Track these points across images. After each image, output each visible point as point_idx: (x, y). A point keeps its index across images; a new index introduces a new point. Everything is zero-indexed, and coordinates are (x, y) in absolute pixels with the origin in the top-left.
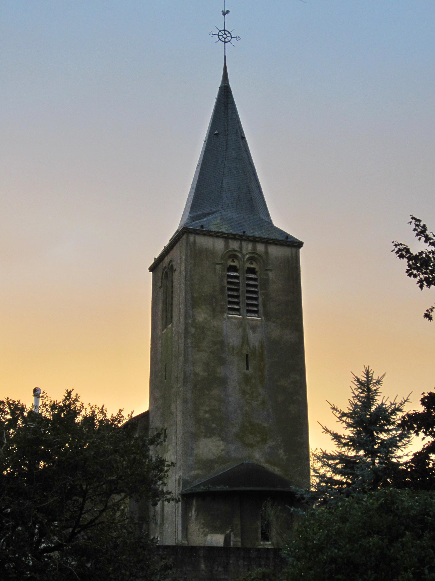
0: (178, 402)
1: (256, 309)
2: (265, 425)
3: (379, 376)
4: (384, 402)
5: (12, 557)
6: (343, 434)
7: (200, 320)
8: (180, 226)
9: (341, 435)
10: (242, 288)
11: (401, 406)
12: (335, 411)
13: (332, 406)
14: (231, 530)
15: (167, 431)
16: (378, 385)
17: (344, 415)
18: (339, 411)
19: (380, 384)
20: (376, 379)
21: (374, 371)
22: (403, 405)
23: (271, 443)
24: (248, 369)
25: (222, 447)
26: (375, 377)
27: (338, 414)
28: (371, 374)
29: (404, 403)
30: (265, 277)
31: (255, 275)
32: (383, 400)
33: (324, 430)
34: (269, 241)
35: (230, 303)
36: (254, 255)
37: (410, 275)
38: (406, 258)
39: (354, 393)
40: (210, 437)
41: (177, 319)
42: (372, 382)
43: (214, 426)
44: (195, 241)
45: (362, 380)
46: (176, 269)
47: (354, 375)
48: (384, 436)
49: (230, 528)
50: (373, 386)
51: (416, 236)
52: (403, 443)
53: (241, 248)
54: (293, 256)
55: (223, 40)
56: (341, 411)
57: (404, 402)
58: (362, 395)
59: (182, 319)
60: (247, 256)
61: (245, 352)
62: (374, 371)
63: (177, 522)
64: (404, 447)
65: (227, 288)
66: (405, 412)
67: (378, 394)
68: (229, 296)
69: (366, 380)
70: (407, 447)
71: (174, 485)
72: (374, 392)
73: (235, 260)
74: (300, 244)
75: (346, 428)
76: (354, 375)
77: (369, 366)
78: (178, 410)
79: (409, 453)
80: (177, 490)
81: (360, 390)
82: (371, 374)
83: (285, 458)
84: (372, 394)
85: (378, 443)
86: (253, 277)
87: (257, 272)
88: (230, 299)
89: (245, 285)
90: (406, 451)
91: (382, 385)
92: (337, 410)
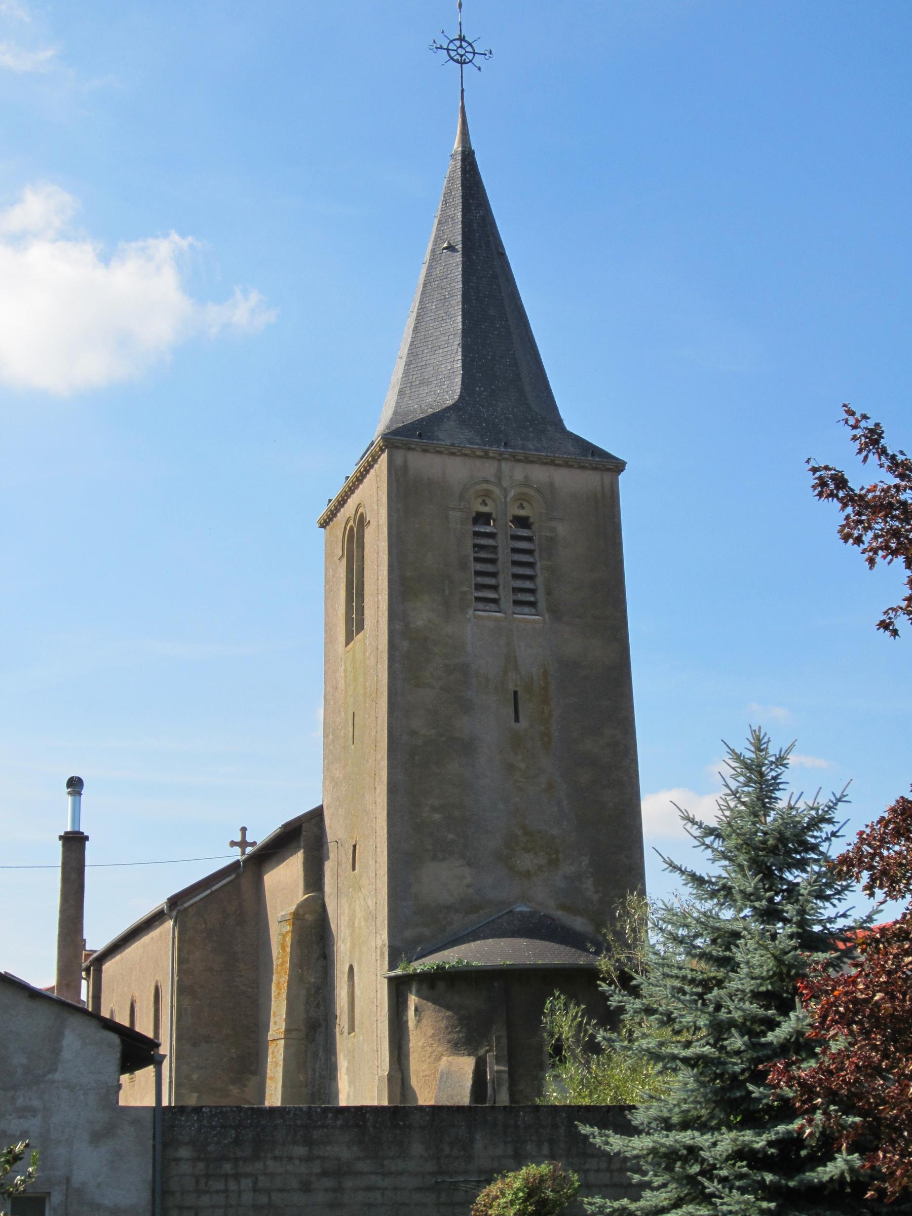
0: (378, 791)
1: (532, 599)
2: (555, 832)
3: (781, 749)
4: (792, 803)
6: (707, 874)
7: (420, 623)
8: (387, 431)
9: (702, 875)
10: (504, 556)
11: (830, 812)
12: (690, 824)
13: (683, 813)
14: (487, 1048)
15: (357, 846)
16: (780, 767)
17: (711, 831)
18: (699, 824)
19: (784, 765)
20: (775, 755)
21: (769, 738)
22: (832, 808)
23: (567, 869)
24: (517, 720)
25: (469, 880)
26: (773, 750)
27: (697, 829)
28: (764, 743)
29: (836, 804)
30: (548, 534)
31: (530, 531)
32: (790, 801)
33: (667, 866)
34: (557, 462)
35: (479, 587)
37: (846, 538)
38: (838, 499)
39: (727, 786)
40: (444, 859)
41: (374, 623)
42: (766, 762)
44: (405, 463)
45: (746, 757)
46: (369, 522)
47: (728, 746)
48: (795, 875)
49: (487, 1044)
50: (769, 770)
51: (858, 453)
52: (836, 889)
53: (499, 477)
55: (464, 44)
56: (701, 823)
57: (835, 801)
58: (746, 789)
59: (383, 622)
60: (512, 493)
61: (511, 687)
62: (769, 738)
63: (379, 1032)
64: (837, 897)
65: (472, 559)
66: (838, 822)
67: (781, 786)
68: (478, 573)
69: (753, 756)
70: (845, 897)
71: (374, 957)
72: (773, 781)
73: (488, 501)
74: (618, 466)
75: (714, 861)
76: (728, 746)
77: (760, 728)
78: (378, 807)
79: (848, 910)
80: (379, 969)
81: (742, 779)
82: (764, 743)
83: (596, 897)
84: (768, 786)
85: (783, 891)
86: (526, 535)
87: (532, 524)
89: (509, 551)
90: (841, 907)
91: (787, 766)
92: (693, 822)
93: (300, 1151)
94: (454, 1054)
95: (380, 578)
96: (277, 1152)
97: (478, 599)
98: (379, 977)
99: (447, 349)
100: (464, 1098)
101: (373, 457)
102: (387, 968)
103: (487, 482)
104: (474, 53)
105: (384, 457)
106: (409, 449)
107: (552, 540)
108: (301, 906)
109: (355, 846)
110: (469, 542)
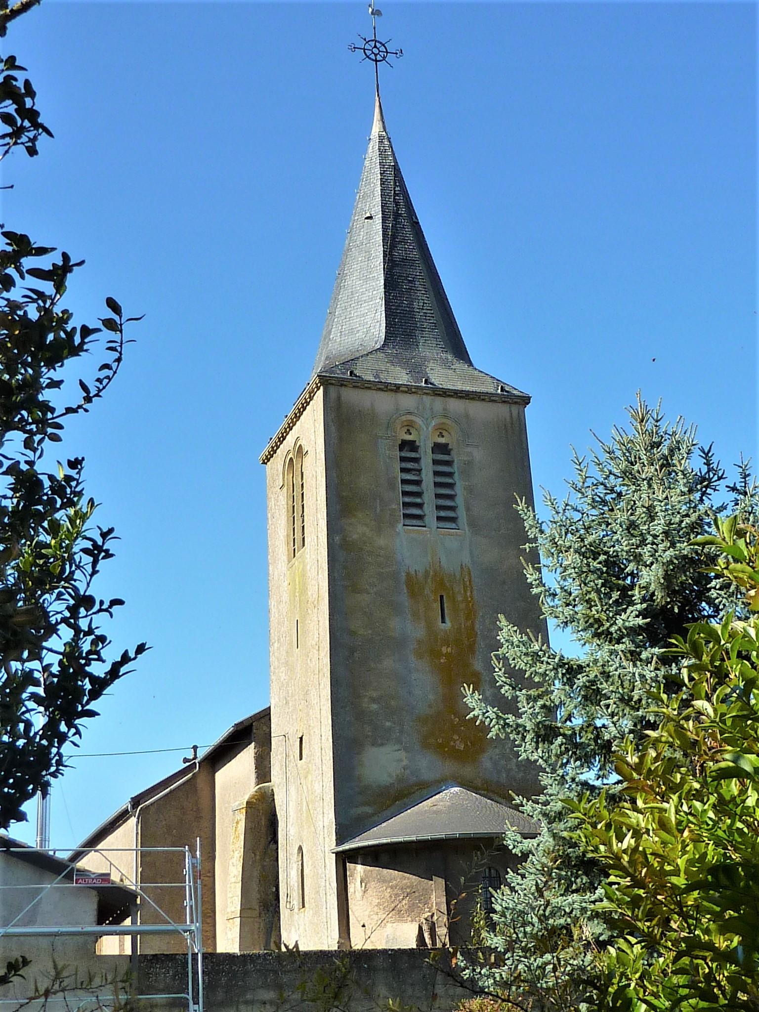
5: (9, 341)
7: (355, 536)
24: (443, 621)
25: (405, 762)
36: (445, 420)
40: (382, 745)
43: (388, 724)
54: (515, 419)
55: (373, 56)
68: (405, 493)
88: (407, 500)
93: (270, 995)
94: (399, 921)
95: (319, 499)
96: (249, 997)
97: (406, 516)
98: (327, 854)
99: (371, 303)
100: (413, 945)
101: (310, 393)
102: (335, 844)
103: (410, 413)
104: (387, 52)
105: (320, 393)
106: (342, 385)
107: (469, 464)
108: (253, 797)
109: (301, 739)
110: (397, 466)
